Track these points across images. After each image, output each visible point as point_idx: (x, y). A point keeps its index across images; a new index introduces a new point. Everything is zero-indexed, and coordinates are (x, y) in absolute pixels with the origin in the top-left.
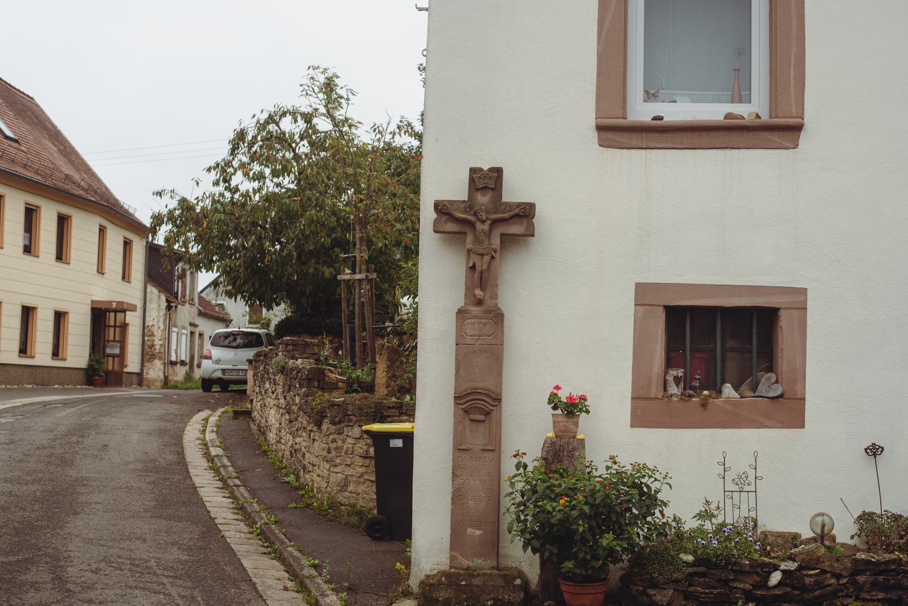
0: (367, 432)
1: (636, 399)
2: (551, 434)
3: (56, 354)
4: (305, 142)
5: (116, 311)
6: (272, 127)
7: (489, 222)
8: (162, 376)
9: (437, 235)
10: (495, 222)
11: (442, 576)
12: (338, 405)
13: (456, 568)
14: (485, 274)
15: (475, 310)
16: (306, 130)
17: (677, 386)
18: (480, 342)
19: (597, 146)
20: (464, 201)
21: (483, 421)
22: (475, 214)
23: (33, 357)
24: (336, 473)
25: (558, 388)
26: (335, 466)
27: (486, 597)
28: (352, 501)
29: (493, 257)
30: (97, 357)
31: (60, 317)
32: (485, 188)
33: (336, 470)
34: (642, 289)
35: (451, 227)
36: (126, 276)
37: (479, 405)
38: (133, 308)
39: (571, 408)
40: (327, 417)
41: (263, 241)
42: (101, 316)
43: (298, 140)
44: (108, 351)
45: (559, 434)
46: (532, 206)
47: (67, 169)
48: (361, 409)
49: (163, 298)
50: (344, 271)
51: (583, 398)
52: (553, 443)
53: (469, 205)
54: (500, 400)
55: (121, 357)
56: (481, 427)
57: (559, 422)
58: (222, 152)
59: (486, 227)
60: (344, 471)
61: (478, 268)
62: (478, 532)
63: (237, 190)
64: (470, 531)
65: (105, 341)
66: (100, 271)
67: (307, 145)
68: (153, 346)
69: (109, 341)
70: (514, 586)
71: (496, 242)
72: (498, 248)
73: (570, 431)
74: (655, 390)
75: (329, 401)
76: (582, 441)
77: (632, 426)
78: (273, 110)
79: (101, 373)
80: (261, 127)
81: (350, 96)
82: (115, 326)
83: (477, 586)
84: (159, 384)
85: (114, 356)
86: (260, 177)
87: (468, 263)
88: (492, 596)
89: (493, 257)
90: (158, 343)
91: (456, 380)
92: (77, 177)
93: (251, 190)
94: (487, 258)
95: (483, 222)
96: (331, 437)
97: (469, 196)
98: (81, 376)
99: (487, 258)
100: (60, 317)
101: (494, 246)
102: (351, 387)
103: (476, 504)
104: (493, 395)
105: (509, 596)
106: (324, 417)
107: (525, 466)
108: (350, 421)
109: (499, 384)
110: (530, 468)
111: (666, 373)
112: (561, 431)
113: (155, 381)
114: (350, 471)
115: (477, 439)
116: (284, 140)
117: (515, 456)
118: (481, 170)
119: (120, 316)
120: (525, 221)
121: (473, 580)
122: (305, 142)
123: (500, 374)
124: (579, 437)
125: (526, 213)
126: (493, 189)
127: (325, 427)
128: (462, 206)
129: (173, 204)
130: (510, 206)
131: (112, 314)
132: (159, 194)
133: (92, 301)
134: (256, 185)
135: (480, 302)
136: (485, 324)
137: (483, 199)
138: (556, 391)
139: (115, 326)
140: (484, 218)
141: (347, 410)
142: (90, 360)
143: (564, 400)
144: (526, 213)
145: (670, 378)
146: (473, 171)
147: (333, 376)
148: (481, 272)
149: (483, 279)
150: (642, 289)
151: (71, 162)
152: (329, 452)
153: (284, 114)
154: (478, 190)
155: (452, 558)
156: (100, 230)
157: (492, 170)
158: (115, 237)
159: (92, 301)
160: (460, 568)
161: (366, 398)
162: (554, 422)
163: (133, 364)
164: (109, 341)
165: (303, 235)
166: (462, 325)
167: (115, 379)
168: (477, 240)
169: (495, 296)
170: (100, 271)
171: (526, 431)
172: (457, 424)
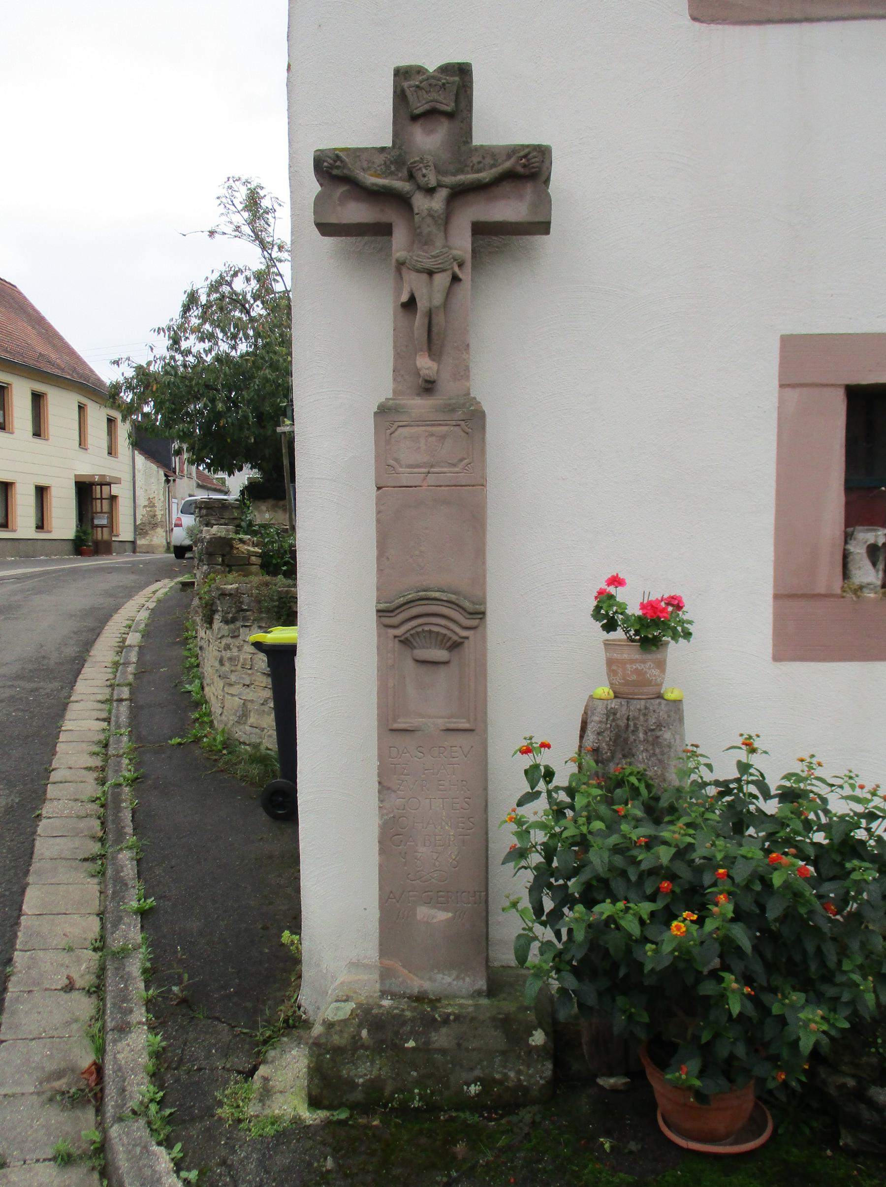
0: (258, 645)
1: (784, 596)
2: (603, 691)
3: (40, 526)
4: (259, 303)
5: (101, 485)
6: (225, 289)
7: (443, 193)
8: (165, 543)
9: (328, 241)
10: (460, 194)
11: (360, 1026)
12: (230, 595)
13: (394, 996)
14: (439, 319)
15: (419, 405)
16: (259, 290)
17: (874, 564)
18: (432, 479)
19: (686, 20)
20: (383, 149)
21: (446, 663)
22: (411, 177)
23: (15, 531)
24: (232, 695)
25: (616, 581)
26: (230, 685)
27: (465, 1076)
28: (255, 739)
29: (455, 279)
31: (41, 492)
32: (431, 114)
33: (232, 690)
34: (794, 348)
35: (356, 212)
37: (433, 627)
38: (118, 481)
39: (655, 627)
40: (217, 611)
41: (217, 402)
42: (86, 491)
43: (252, 302)
44: (96, 522)
45: (625, 689)
46: (543, 152)
47: (41, 348)
48: (259, 602)
49: (162, 473)
50: (284, 422)
51: (676, 603)
52: (611, 713)
53: (397, 157)
54: (483, 613)
55: (111, 526)
56: (442, 674)
57: (622, 663)
58: (172, 313)
59: (437, 203)
60: (240, 694)
61: (422, 304)
62: (443, 916)
63: (188, 352)
64: (423, 912)
65: (93, 513)
66: (82, 443)
67: (261, 306)
68: (155, 516)
69: (97, 513)
70: (530, 1050)
71: (462, 241)
72: (468, 256)
73: (648, 683)
74: (827, 577)
75: (218, 589)
76: (677, 703)
77: (778, 657)
78: (223, 269)
79: (88, 542)
80: (214, 287)
81: (276, 206)
82: (101, 499)
83: (443, 1051)
84: (163, 549)
85: (102, 527)
86: (211, 337)
87: (398, 294)
88: (477, 1073)
89: (455, 279)
90: (159, 513)
91: (380, 570)
92: (53, 356)
93: (202, 351)
94: (442, 280)
95: (430, 191)
96: (224, 641)
97: (396, 135)
98: (69, 547)
99: (442, 280)
100: (41, 492)
101: (456, 252)
102: (282, 558)
103: (436, 851)
104: (467, 604)
105: (519, 1072)
106: (214, 612)
107: (549, 775)
108: (245, 619)
109: (479, 579)
110: (561, 779)
111: (848, 537)
112: (627, 683)
113: (159, 546)
114: (249, 694)
115: (432, 703)
116: (239, 302)
117: (527, 751)
118: (420, 70)
119: (105, 489)
120: (529, 189)
121: (434, 1036)
122: (259, 303)
123: (480, 553)
124: (671, 695)
125: (528, 169)
126: (450, 115)
127: (217, 624)
128: (379, 160)
129: (130, 373)
130: (489, 153)
131: (98, 487)
132: (117, 363)
134: (207, 345)
135: (428, 387)
136: (443, 437)
137: (429, 141)
138: (612, 589)
139: (101, 499)
140: (433, 183)
141: (242, 603)
142: (77, 531)
143: (634, 610)
144: (528, 169)
145: (858, 549)
146: (401, 74)
147: (244, 548)
148: (430, 315)
149: (435, 330)
150: (794, 348)
151: (54, 346)
152: (221, 663)
153: (235, 274)
154: (415, 118)
155: (386, 974)
157: (446, 69)
158: (97, 415)
160: (403, 996)
161: (267, 584)
162: (610, 662)
163: (125, 532)
164: (97, 513)
165: (258, 395)
166: (388, 442)
167: (102, 548)
168: (418, 238)
169: (463, 373)
170: (82, 443)
171: (543, 686)
172: (385, 671)
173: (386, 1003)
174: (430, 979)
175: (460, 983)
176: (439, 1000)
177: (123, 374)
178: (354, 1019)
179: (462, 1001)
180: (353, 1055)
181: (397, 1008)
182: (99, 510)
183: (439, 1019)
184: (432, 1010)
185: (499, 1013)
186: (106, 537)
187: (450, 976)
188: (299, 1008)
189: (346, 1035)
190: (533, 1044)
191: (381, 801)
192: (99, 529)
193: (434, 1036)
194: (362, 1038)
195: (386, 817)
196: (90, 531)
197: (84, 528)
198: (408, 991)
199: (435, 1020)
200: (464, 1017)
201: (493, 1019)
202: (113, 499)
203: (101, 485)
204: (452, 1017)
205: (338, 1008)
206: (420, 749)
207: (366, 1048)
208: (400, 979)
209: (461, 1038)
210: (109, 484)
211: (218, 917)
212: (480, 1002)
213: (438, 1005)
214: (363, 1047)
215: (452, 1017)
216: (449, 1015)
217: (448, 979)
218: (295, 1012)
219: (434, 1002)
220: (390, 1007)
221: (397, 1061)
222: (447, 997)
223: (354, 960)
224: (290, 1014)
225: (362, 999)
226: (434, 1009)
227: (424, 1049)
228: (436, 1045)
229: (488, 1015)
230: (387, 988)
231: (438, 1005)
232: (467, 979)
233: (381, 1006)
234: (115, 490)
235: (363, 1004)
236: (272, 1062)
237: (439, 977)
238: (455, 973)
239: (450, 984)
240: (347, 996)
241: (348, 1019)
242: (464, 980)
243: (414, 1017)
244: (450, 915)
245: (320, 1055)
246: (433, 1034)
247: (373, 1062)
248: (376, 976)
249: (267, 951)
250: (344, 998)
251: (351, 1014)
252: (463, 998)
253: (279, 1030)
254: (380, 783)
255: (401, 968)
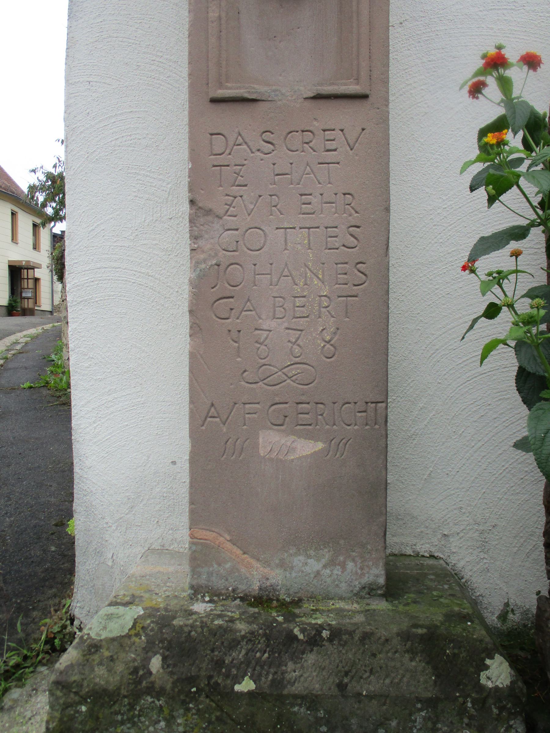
5: (28, 269)
11: (149, 650)
13: (216, 595)
30: (14, 298)
36: (36, 247)
44: (24, 295)
55: (35, 298)
62: (306, 448)
64: (270, 441)
65: (21, 289)
66: (14, 238)
69: (24, 289)
70: (485, 697)
82: (28, 279)
83: (311, 701)
85: (28, 298)
98: (4, 311)
121: (291, 670)
131: (26, 271)
132: (34, 171)
133: (9, 261)
139: (28, 279)
142: (10, 300)
155: (200, 555)
156: (12, 214)
159: (9, 261)
160: (233, 595)
164: (24, 289)
170: (14, 238)
173: (200, 607)
174: (282, 565)
175: (337, 571)
176: (298, 603)
177: (38, 178)
178: (137, 635)
179: (341, 605)
180: (132, 707)
181: (220, 616)
182: (26, 287)
183: (301, 637)
184: (286, 620)
185: (416, 626)
186: (31, 305)
187: (318, 560)
188: (72, 620)
189: (120, 668)
190: (490, 684)
191: (195, 237)
192: (26, 300)
193: (291, 670)
194: (151, 673)
195: (203, 266)
196: (19, 300)
197: (14, 298)
198: (242, 587)
199: (293, 638)
200: (351, 634)
201: (405, 636)
202: (37, 280)
203: (28, 269)
204: (325, 634)
205: (110, 617)
206: (267, 136)
207: (160, 693)
208: (228, 565)
209: (346, 674)
210: (33, 268)
211: (6, 514)
212: (372, 607)
213: (297, 611)
214: (150, 690)
215: (325, 634)
216: (319, 629)
217: (314, 565)
218: (64, 627)
219: (290, 606)
220: (208, 615)
221: (218, 719)
222: (312, 597)
223: (156, 546)
224: (56, 629)
225: (159, 602)
226: (290, 617)
227: (273, 695)
228: (297, 689)
229: (395, 629)
230: (203, 580)
231: (297, 611)
232: (350, 565)
233: (191, 613)
234: (38, 273)
235: (158, 610)
236: (11, 708)
237: (298, 561)
238: (327, 555)
239: (318, 573)
240: (133, 596)
241: (128, 636)
242: (343, 566)
243: (252, 633)
244: (320, 445)
245: (67, 706)
246: (290, 665)
247: (170, 720)
248: (187, 568)
249: (53, 549)
250: (127, 599)
251: (134, 626)
252: (341, 598)
253: (38, 655)
254: (192, 202)
255: (229, 545)
